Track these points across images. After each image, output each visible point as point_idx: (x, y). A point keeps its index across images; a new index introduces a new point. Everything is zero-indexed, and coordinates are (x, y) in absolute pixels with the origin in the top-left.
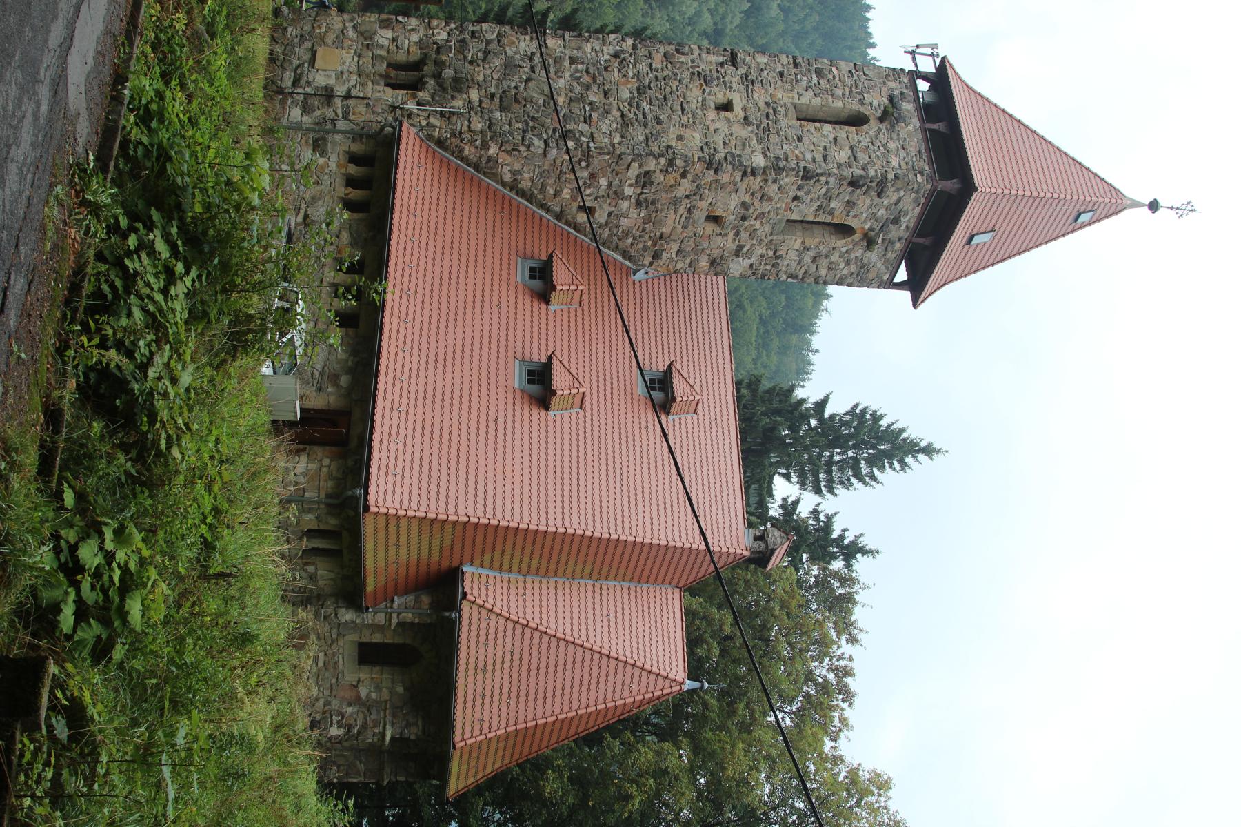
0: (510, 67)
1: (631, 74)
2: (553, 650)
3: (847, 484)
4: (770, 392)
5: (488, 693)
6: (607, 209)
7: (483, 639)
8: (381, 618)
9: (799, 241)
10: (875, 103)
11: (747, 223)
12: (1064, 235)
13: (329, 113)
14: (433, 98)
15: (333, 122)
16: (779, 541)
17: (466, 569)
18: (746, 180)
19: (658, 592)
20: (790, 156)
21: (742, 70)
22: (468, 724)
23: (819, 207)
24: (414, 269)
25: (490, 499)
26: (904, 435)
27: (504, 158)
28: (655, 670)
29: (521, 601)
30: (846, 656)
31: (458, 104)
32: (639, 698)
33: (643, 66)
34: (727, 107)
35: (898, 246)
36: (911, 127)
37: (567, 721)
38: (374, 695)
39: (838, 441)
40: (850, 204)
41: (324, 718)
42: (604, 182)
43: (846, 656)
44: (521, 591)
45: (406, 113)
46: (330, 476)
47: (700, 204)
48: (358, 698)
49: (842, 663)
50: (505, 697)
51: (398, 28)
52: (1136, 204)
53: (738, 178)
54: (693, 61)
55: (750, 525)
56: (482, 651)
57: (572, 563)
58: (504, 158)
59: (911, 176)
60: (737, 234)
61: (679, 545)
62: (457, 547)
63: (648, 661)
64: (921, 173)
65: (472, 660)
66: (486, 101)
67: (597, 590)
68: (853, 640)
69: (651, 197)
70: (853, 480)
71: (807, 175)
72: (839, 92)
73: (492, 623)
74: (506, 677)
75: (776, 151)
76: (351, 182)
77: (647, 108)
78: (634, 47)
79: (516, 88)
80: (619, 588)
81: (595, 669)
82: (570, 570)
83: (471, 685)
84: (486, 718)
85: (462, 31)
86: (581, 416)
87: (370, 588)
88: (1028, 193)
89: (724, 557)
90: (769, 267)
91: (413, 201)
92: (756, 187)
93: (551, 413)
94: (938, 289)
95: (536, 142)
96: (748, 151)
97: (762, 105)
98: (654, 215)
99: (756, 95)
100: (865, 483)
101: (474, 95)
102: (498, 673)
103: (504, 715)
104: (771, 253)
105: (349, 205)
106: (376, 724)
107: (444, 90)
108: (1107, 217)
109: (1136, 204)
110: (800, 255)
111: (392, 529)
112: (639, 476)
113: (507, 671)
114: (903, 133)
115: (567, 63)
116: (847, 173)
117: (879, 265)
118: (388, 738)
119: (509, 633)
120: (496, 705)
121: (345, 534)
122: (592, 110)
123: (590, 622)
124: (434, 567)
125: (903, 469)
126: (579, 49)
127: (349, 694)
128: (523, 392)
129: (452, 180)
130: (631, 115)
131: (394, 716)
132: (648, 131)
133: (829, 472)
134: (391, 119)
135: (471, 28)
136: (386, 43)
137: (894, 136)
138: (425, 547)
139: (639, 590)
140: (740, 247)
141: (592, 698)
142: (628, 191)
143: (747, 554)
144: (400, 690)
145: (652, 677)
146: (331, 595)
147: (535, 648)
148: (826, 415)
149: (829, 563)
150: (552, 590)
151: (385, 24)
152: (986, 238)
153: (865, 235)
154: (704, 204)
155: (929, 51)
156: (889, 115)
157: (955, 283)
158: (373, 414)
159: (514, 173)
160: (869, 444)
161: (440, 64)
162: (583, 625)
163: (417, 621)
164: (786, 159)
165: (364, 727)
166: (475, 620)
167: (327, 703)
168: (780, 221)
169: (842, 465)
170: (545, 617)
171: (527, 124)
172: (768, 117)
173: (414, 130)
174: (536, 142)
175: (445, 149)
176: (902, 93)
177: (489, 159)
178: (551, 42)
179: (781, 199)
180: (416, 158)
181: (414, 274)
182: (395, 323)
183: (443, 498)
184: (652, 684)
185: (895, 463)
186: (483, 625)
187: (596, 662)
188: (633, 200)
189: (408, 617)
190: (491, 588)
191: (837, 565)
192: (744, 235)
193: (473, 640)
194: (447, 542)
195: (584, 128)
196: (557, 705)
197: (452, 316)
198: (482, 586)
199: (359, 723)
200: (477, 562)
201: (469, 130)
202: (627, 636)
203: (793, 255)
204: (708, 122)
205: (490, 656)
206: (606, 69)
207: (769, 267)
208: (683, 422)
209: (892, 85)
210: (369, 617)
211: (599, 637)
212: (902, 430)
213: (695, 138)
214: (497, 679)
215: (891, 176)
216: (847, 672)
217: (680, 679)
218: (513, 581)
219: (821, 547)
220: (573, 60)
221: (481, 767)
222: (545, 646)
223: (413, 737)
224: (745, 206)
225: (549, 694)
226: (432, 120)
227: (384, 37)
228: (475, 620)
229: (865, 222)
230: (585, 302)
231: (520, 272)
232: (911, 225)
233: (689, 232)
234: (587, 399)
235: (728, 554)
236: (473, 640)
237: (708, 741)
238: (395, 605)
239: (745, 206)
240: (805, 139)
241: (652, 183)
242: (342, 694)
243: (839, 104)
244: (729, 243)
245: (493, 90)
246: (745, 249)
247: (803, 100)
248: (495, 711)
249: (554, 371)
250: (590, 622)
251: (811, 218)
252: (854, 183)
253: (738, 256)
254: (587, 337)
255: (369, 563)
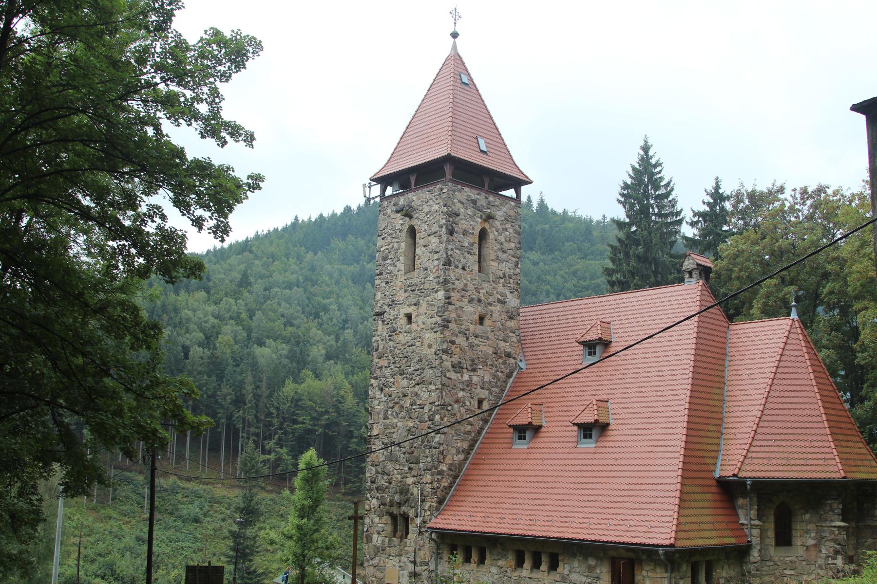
0: (392, 459)
1: (392, 380)
2: (773, 412)
3: (673, 203)
4: (613, 261)
5: (805, 455)
6: (479, 390)
7: (765, 461)
8: (756, 532)
9: (492, 263)
10: (401, 222)
11: (483, 298)
12: (478, 91)
13: (425, 575)
14: (413, 507)
15: (430, 572)
16: (691, 261)
17: (717, 475)
18: (453, 302)
19: (732, 341)
20: (436, 275)
21: (386, 308)
22: (827, 469)
23: (469, 253)
24: (520, 517)
25: (666, 462)
26: (637, 166)
27: (448, 460)
28: (784, 340)
29: (739, 436)
30: (793, 193)
31: (416, 491)
32: (805, 350)
33: (387, 372)
34: (409, 317)
35: (491, 198)
36: (414, 198)
37: (824, 399)
38: (813, 535)
39: (645, 211)
40: (465, 233)
41: (831, 569)
42: (461, 394)
43: (793, 193)
44: (732, 436)
45: (423, 525)
46: (654, 570)
47: (471, 331)
48: (815, 545)
49: (798, 196)
50: (807, 444)
51: (372, 530)
52: (454, 47)
53: (453, 307)
54: (382, 340)
55: (681, 281)
56: (774, 461)
57: (711, 402)
58: (448, 460)
59: (444, 196)
60: (490, 304)
61: (696, 330)
62: (701, 482)
63: (778, 345)
64: (442, 190)
65: (781, 468)
66: (414, 473)
67: (731, 383)
68: (781, 190)
69: (469, 362)
70: (670, 198)
71: (448, 263)
72: (396, 245)
73: (754, 455)
74: (793, 443)
75: (434, 284)
76: (467, 560)
77: (412, 368)
78: (376, 378)
79: (404, 453)
80: (730, 368)
81: (785, 382)
82: (717, 403)
83: (799, 468)
84: (823, 456)
85: (371, 490)
86: (612, 401)
87: (733, 541)
88: (450, 119)
89: (703, 298)
90: (512, 281)
91: (477, 519)
92: (458, 295)
93: (611, 421)
94: (518, 168)
95: (437, 439)
96: (435, 302)
97: (407, 294)
98: (481, 360)
99: (401, 299)
100: (672, 190)
101: (410, 481)
102: (790, 449)
103: (820, 444)
104: (502, 281)
105: (482, 561)
106: (832, 533)
107: (407, 500)
108: (464, 64)
109: (454, 47)
110: (502, 262)
111: (687, 527)
112: (651, 360)
113: (788, 443)
114: (418, 202)
115: (387, 421)
116: (445, 237)
117: (505, 209)
118: (842, 524)
119: (761, 443)
120: (813, 450)
121: (694, 559)
122: (415, 404)
123: (753, 387)
124: (717, 497)
125: (660, 165)
126: (379, 414)
127: (813, 553)
128: (597, 442)
129: (464, 493)
130: (417, 378)
131: (826, 520)
132: (427, 368)
133: (666, 215)
134: (427, 535)
135: (369, 484)
136: (381, 538)
137: (420, 208)
138: (701, 504)
139: (731, 354)
140: (499, 301)
141: (807, 382)
142: (466, 377)
143: (701, 282)
144: (807, 516)
145: (789, 341)
146: (742, 567)
147: (771, 424)
148: (627, 220)
149: (727, 212)
150: (731, 414)
151: (369, 539)
152: (482, 142)
153: (485, 220)
154: (472, 327)
155: (367, 189)
156: (407, 212)
157: (514, 158)
158: (611, 542)
159: (458, 452)
160: (645, 186)
161: (392, 504)
162: (755, 392)
163: (756, 507)
164: (439, 277)
165: (835, 541)
166: (752, 468)
167: (820, 567)
168: (479, 277)
169: (661, 207)
170: (749, 419)
171: (426, 445)
172: (413, 291)
173: (433, 518)
174: (437, 439)
175: (444, 499)
176: (394, 205)
177: (450, 469)
178: (375, 432)
179: (461, 278)
180: (450, 517)
181: (523, 517)
182: (554, 529)
183: (666, 494)
184: (794, 341)
185: (657, 170)
186: (756, 461)
187: (780, 382)
188: (472, 374)
189: (753, 513)
190: (730, 457)
191: (728, 205)
192: (491, 299)
193: (767, 468)
194: (697, 489)
195: (427, 408)
196: (812, 406)
197: (550, 491)
198: (729, 464)
199: (832, 544)
200: (712, 468)
201: (431, 483)
202: (762, 361)
203: (502, 266)
204: (419, 329)
205: (778, 455)
206: (390, 396)
207: (512, 281)
208: (616, 331)
209: (389, 211)
210: (755, 540)
211: (763, 381)
212: (634, 169)
213: (429, 336)
214: (794, 449)
215: (445, 209)
216: (804, 191)
217: (790, 322)
218: (726, 442)
219: (716, 218)
220: (386, 418)
221: (863, 457)
222: (769, 418)
223: (841, 507)
224: (471, 301)
225: (804, 412)
226: (426, 508)
227: (377, 540)
228: (752, 468)
229: (476, 222)
230: (540, 401)
231: (521, 446)
232: (477, 192)
233: (491, 335)
234: (601, 398)
235: (702, 295)
236: (767, 468)
237: (855, 289)
238: (745, 522)
239: (471, 301)
240: (426, 266)
241: (460, 363)
242: (813, 557)
243: (403, 244)
244: (497, 308)
245: (406, 469)
246: (500, 298)
247: (402, 268)
248: (817, 450)
249: (583, 421)
250: (753, 387)
251: (477, 257)
252: (451, 232)
253: (505, 302)
254: (562, 399)
255: (713, 542)
